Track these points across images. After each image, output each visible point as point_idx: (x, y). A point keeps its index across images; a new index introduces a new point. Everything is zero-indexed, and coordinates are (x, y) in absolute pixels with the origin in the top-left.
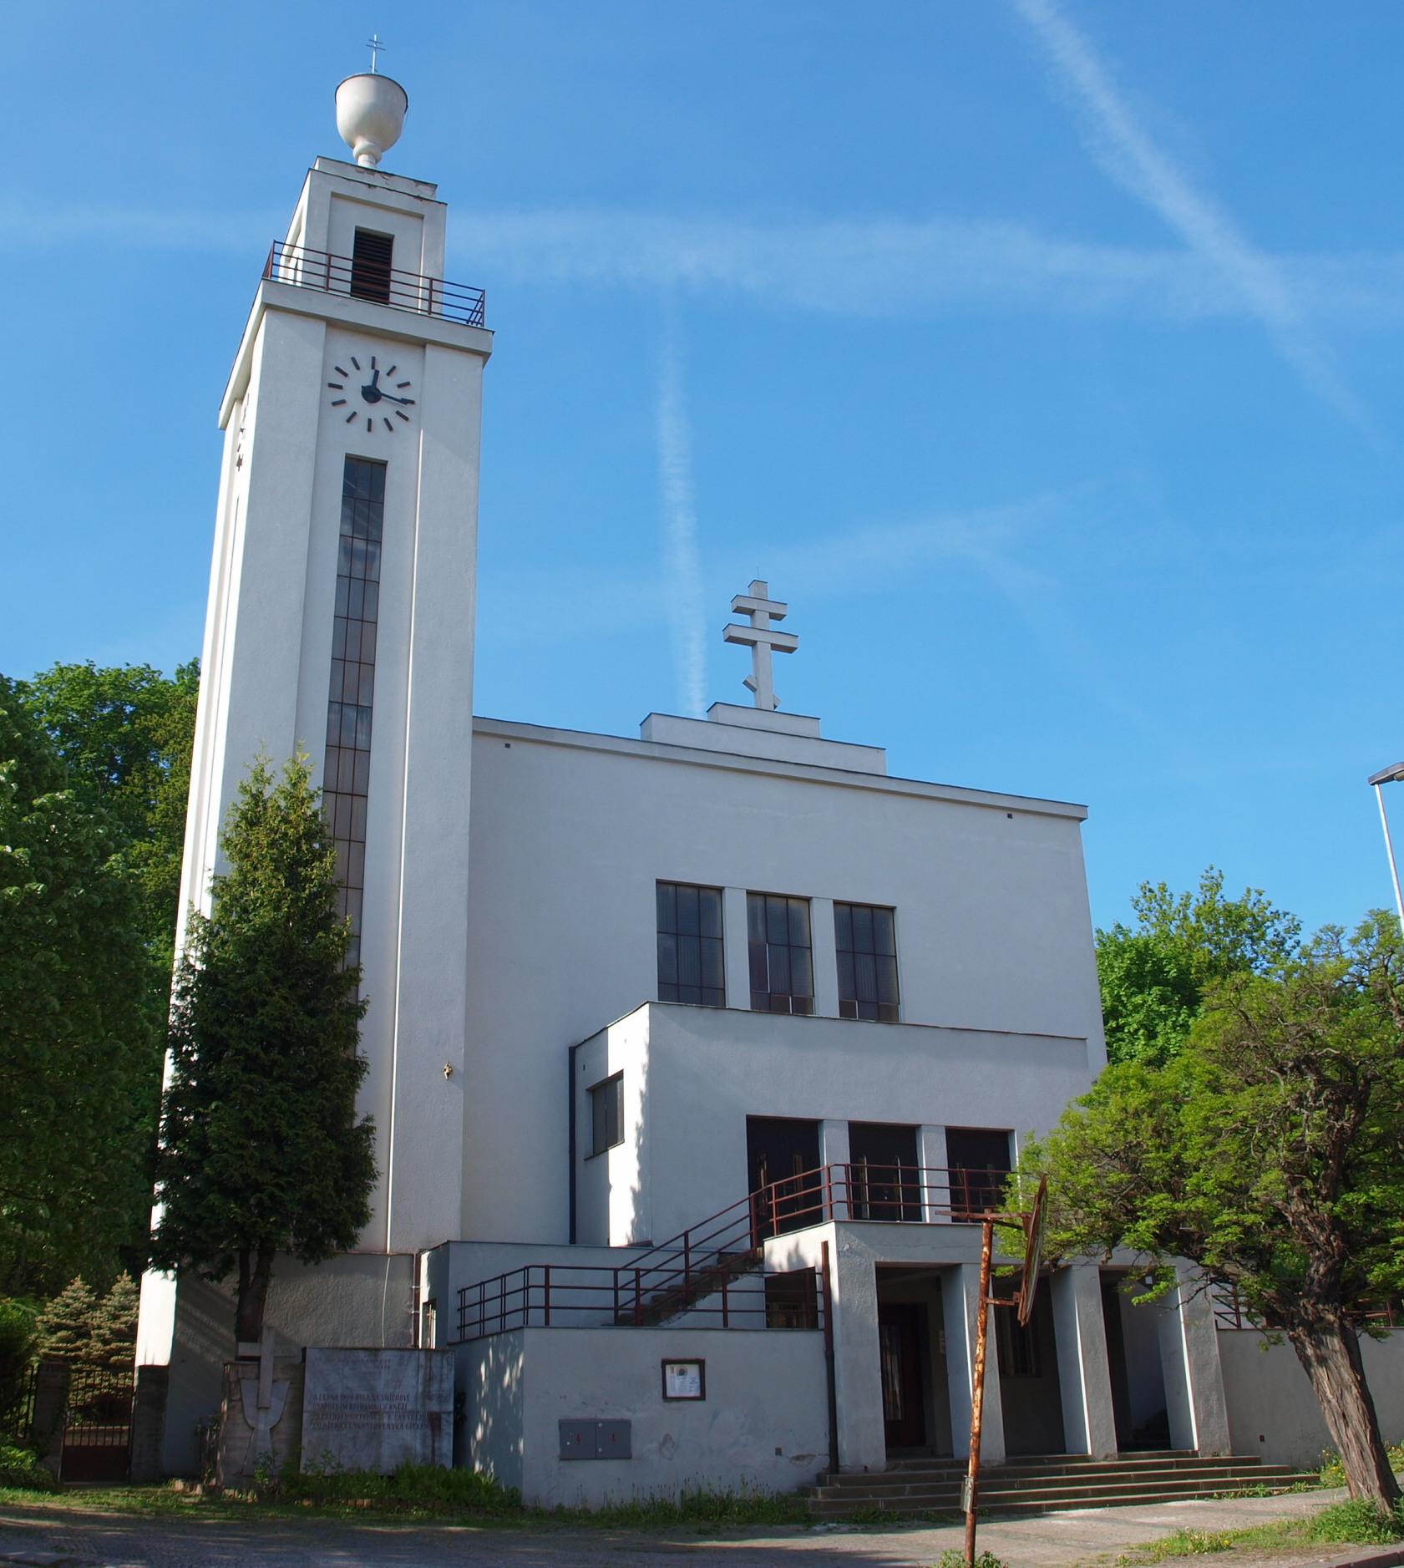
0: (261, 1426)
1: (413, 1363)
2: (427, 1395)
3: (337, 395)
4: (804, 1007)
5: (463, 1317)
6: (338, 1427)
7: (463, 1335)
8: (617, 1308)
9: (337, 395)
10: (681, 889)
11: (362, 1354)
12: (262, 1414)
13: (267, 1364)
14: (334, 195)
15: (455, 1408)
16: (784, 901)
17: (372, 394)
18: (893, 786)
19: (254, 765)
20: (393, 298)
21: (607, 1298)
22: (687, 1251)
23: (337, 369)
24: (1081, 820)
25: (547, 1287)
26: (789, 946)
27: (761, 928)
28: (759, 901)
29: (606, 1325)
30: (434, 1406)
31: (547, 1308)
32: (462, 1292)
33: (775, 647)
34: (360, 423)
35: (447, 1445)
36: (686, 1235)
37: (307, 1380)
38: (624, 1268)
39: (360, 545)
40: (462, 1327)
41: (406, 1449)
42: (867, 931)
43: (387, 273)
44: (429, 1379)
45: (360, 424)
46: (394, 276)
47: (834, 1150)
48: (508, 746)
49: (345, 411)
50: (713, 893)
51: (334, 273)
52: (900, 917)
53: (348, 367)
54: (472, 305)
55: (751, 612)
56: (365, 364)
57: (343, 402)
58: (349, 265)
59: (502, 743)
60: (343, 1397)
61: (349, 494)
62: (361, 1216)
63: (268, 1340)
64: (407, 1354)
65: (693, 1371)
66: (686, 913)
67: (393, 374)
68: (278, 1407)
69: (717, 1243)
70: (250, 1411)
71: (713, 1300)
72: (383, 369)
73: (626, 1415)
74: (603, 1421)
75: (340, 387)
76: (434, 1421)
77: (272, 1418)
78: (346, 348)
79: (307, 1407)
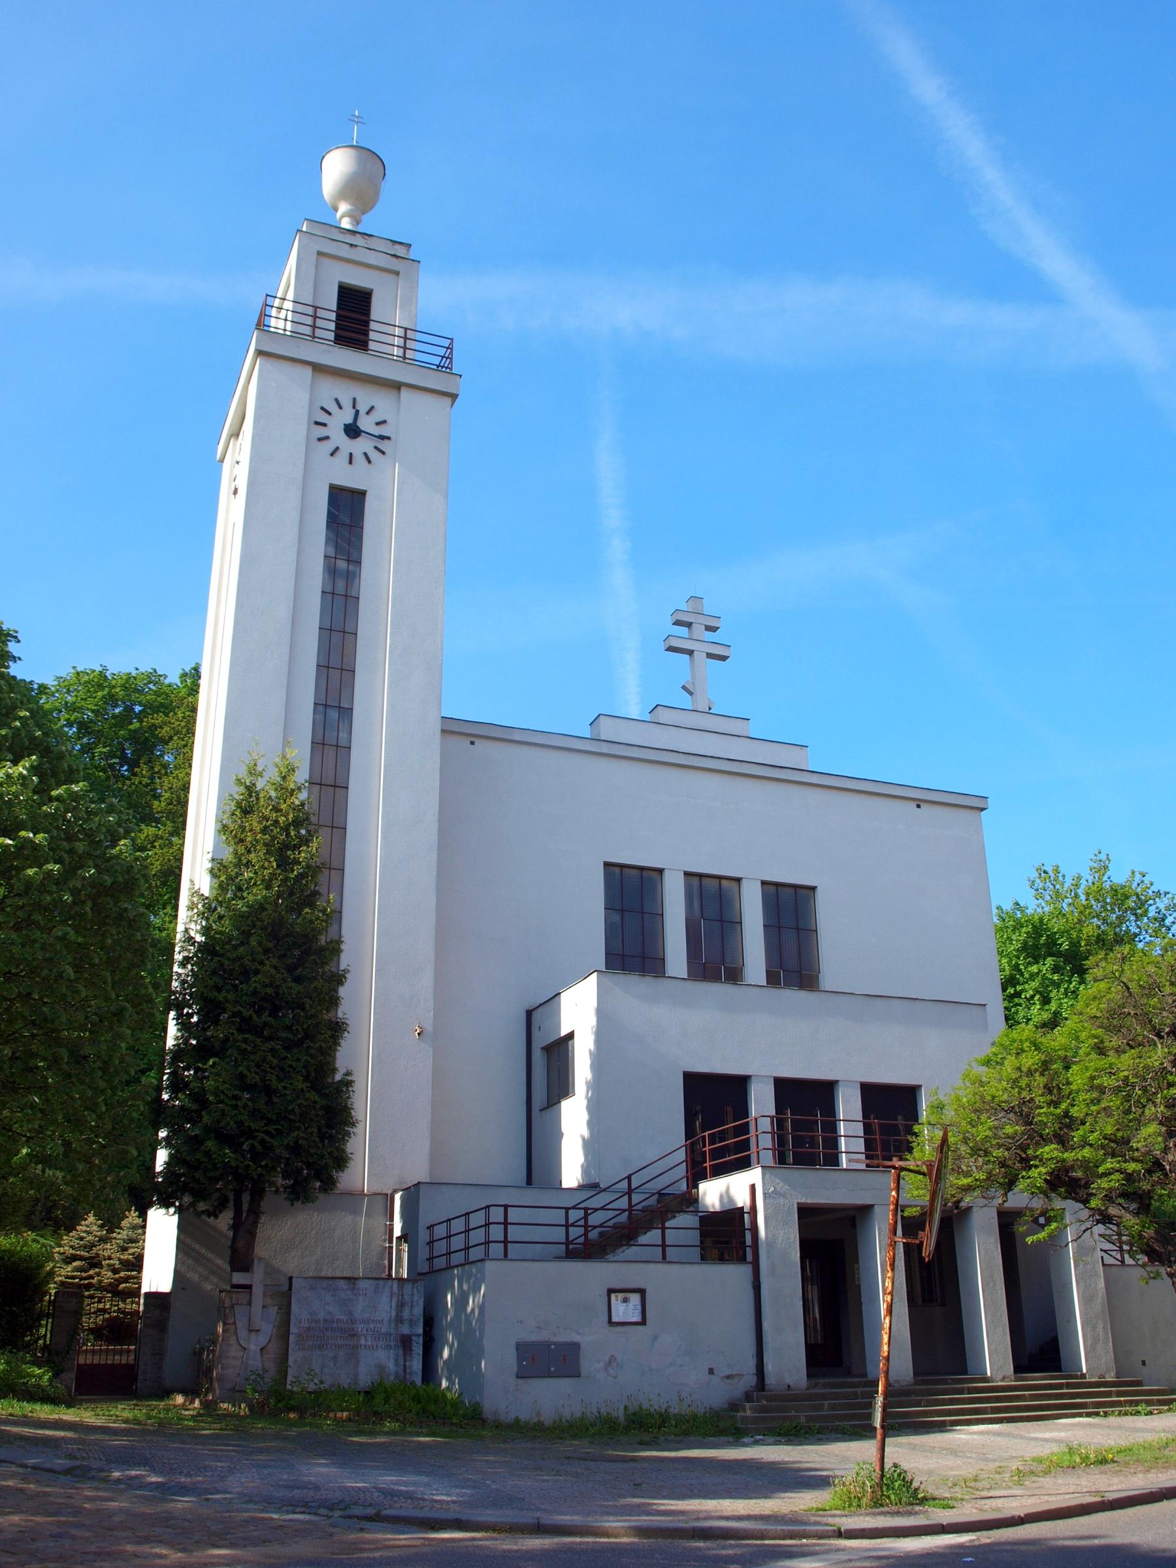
0: (253, 1347)
1: (387, 1292)
2: (399, 1320)
3: (322, 432)
4: (734, 975)
5: (431, 1250)
6: (321, 1347)
7: (431, 1266)
8: (568, 1243)
11: (342, 1283)
12: (253, 1335)
13: (258, 1291)
14: (320, 253)
17: (353, 431)
18: (814, 779)
20: (372, 345)
21: (559, 1234)
22: (630, 1192)
23: (322, 408)
24: (982, 809)
26: (721, 921)
29: (558, 1258)
30: (405, 1330)
33: (710, 656)
35: (417, 1364)
36: (629, 1178)
38: (574, 1208)
39: (342, 564)
40: (431, 1259)
41: (381, 1368)
42: (791, 907)
43: (366, 323)
44: (401, 1306)
46: (373, 325)
47: (761, 1103)
48: (472, 743)
49: (328, 446)
50: (655, 875)
51: (319, 323)
52: (820, 895)
54: (442, 351)
55: (689, 625)
56: (346, 403)
57: (327, 438)
60: (325, 1321)
61: (333, 520)
62: (341, 1161)
64: (381, 1282)
65: (635, 1299)
66: (630, 893)
67: (373, 413)
68: (267, 1329)
70: (243, 1333)
71: (653, 1236)
72: (363, 408)
73: (576, 1338)
74: (556, 1344)
75: (325, 425)
76: (405, 1343)
77: (262, 1339)
78: (330, 390)
79: (293, 1329)
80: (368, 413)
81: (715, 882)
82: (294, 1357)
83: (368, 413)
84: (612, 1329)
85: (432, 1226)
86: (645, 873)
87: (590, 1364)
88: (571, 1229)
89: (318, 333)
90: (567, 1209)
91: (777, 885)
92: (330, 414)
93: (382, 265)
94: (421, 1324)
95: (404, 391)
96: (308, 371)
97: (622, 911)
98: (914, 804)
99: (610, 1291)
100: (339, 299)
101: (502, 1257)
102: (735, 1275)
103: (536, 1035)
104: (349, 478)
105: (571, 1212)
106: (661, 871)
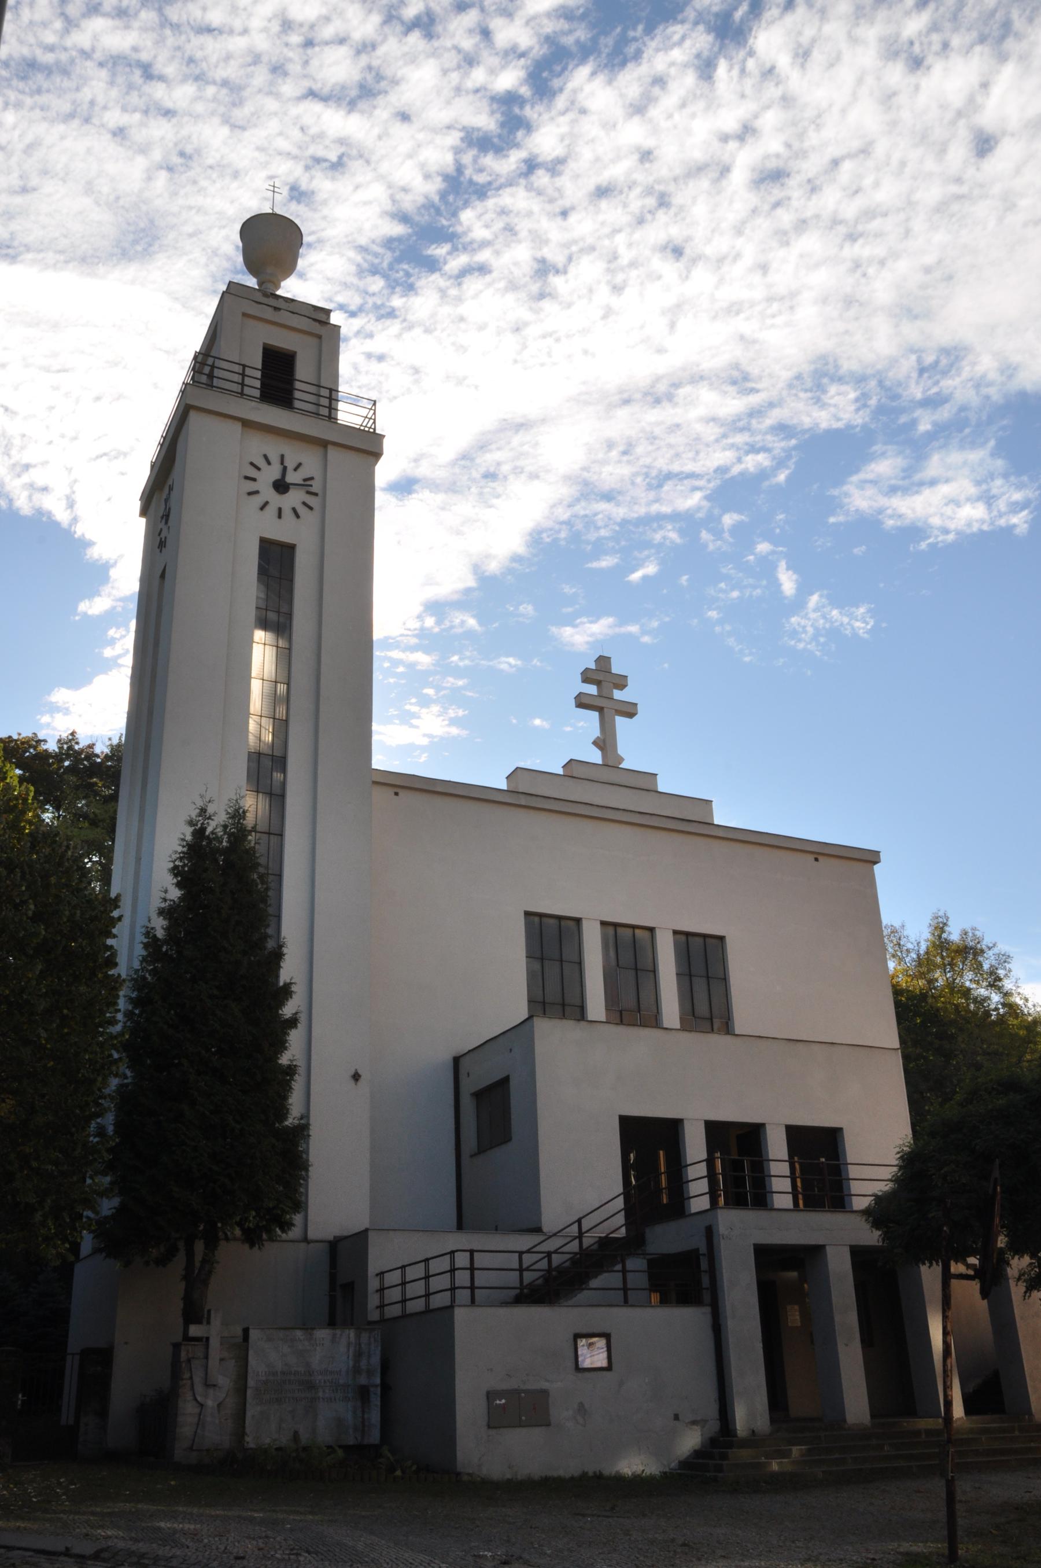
0: (210, 1403)
2: (356, 1370)
3: (251, 486)
4: (654, 1021)
5: (382, 1298)
7: (382, 1314)
8: (522, 1287)
9: (251, 486)
10: (545, 920)
12: (211, 1391)
13: (214, 1343)
14: (244, 315)
15: (382, 1380)
16: (631, 930)
17: (281, 486)
19: (200, 803)
20: (297, 404)
21: (513, 1279)
22: (580, 1235)
23: (252, 464)
24: (875, 863)
25: (472, 1269)
27: (612, 953)
28: (611, 930)
29: (505, 1304)
30: (363, 1380)
31: (472, 1288)
32: (381, 1274)
34: (272, 510)
35: (375, 1416)
36: (579, 1221)
37: (250, 1358)
38: (528, 1251)
40: (382, 1306)
42: (704, 958)
44: (358, 1355)
45: (271, 511)
48: (396, 794)
49: (258, 500)
50: (571, 923)
51: (247, 381)
53: (261, 462)
54: (364, 412)
56: (275, 459)
57: (257, 492)
58: (258, 374)
59: (391, 791)
60: (283, 1373)
62: (299, 1205)
63: (216, 1321)
65: (601, 1343)
66: (551, 940)
67: (300, 470)
68: (225, 1381)
69: (600, 1233)
70: (199, 1388)
72: (290, 464)
73: (545, 1385)
74: (526, 1391)
75: (254, 480)
76: (363, 1394)
78: (258, 446)
79: (251, 1383)
80: (295, 470)
81: (629, 931)
82: (252, 1411)
83: (295, 470)
84: (580, 1375)
85: (382, 1273)
86: (563, 923)
87: (561, 1413)
88: (525, 1273)
89: (247, 390)
90: (521, 1253)
91: (688, 934)
92: (259, 469)
93: (305, 328)
94: (379, 1375)
95: (332, 451)
96: (238, 426)
97: (542, 959)
98: (811, 857)
99: (577, 1336)
100: (264, 357)
101: (469, 1302)
102: (687, 1321)
103: (464, 1082)
104: (282, 532)
105: (524, 1256)
106: (578, 921)
